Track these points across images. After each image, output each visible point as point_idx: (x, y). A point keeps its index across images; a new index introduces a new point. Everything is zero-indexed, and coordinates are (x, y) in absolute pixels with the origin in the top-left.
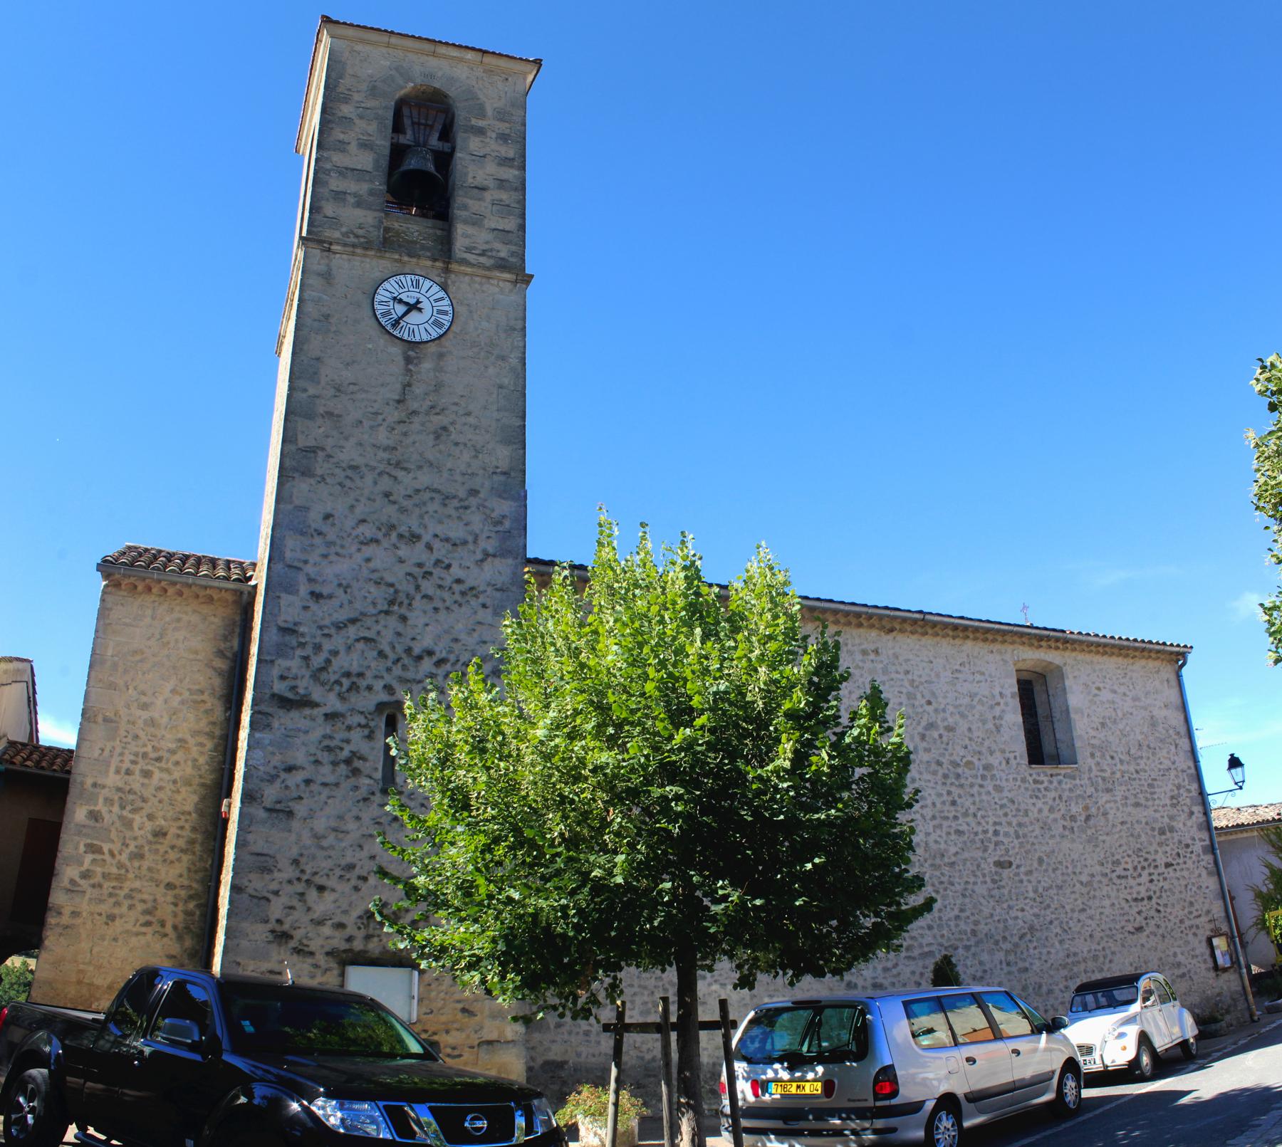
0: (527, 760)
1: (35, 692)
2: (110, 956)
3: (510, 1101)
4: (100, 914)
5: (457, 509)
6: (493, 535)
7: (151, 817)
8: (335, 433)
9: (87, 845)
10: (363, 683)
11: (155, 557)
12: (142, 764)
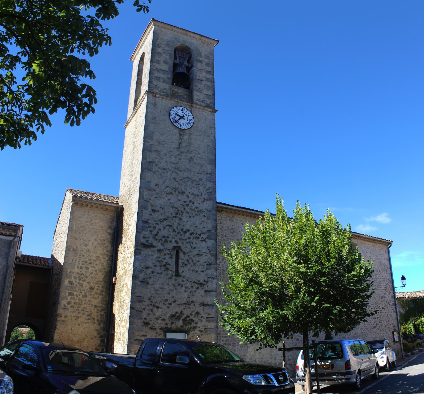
2: (78, 331)
4: (74, 316)
5: (196, 184)
6: (206, 193)
7: (89, 283)
9: (69, 293)
12: (85, 265)
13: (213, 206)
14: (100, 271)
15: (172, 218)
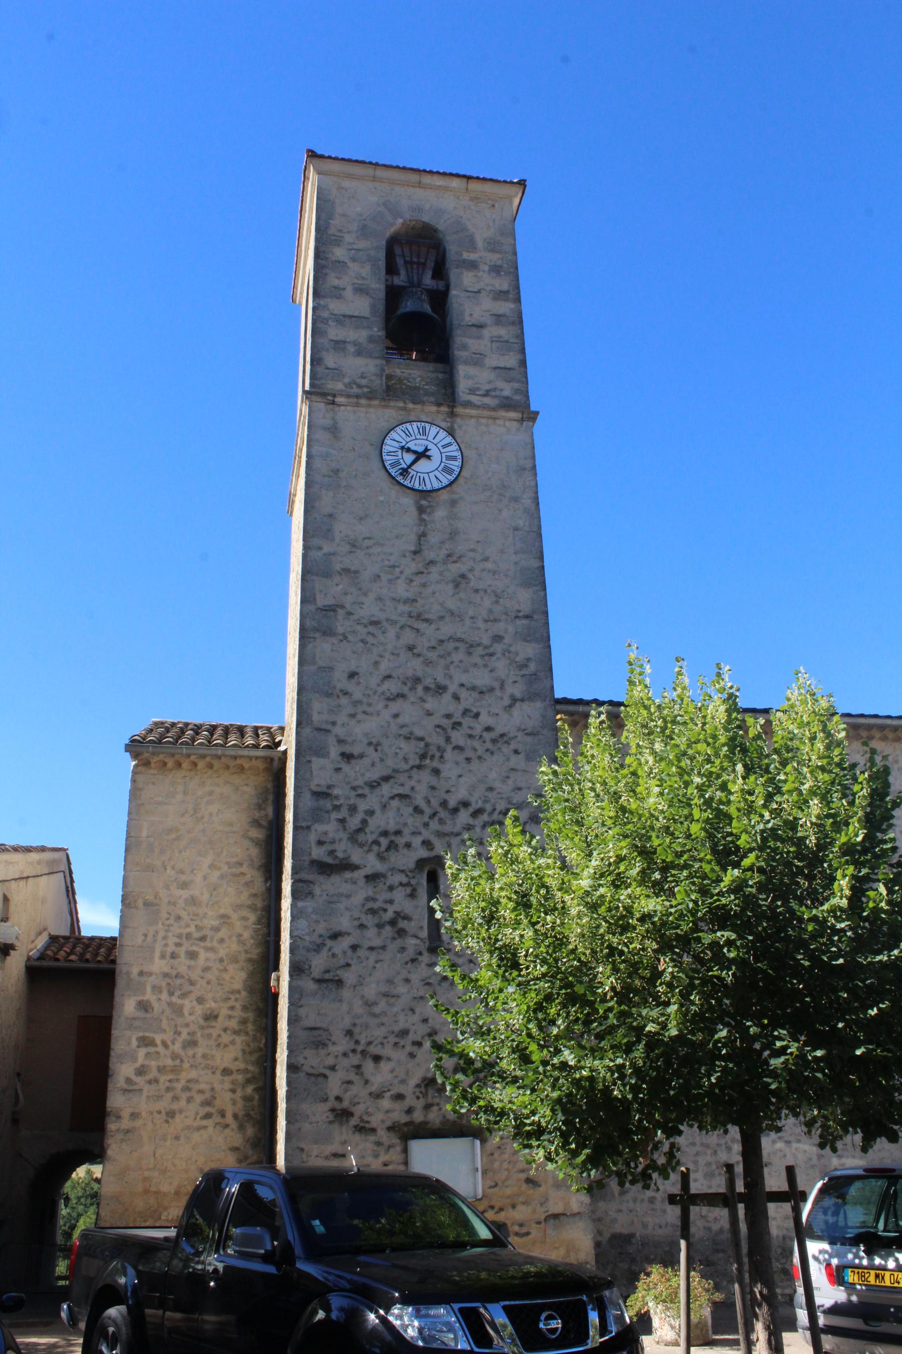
0: (574, 912)
1: (72, 881)
3: (582, 1295)
4: (159, 1112)
5: (482, 656)
6: (519, 679)
7: (200, 1000)
8: (353, 590)
10: (401, 841)
11: (182, 731)
12: (187, 946)
13: (544, 716)
14: (234, 960)
15: (407, 771)
